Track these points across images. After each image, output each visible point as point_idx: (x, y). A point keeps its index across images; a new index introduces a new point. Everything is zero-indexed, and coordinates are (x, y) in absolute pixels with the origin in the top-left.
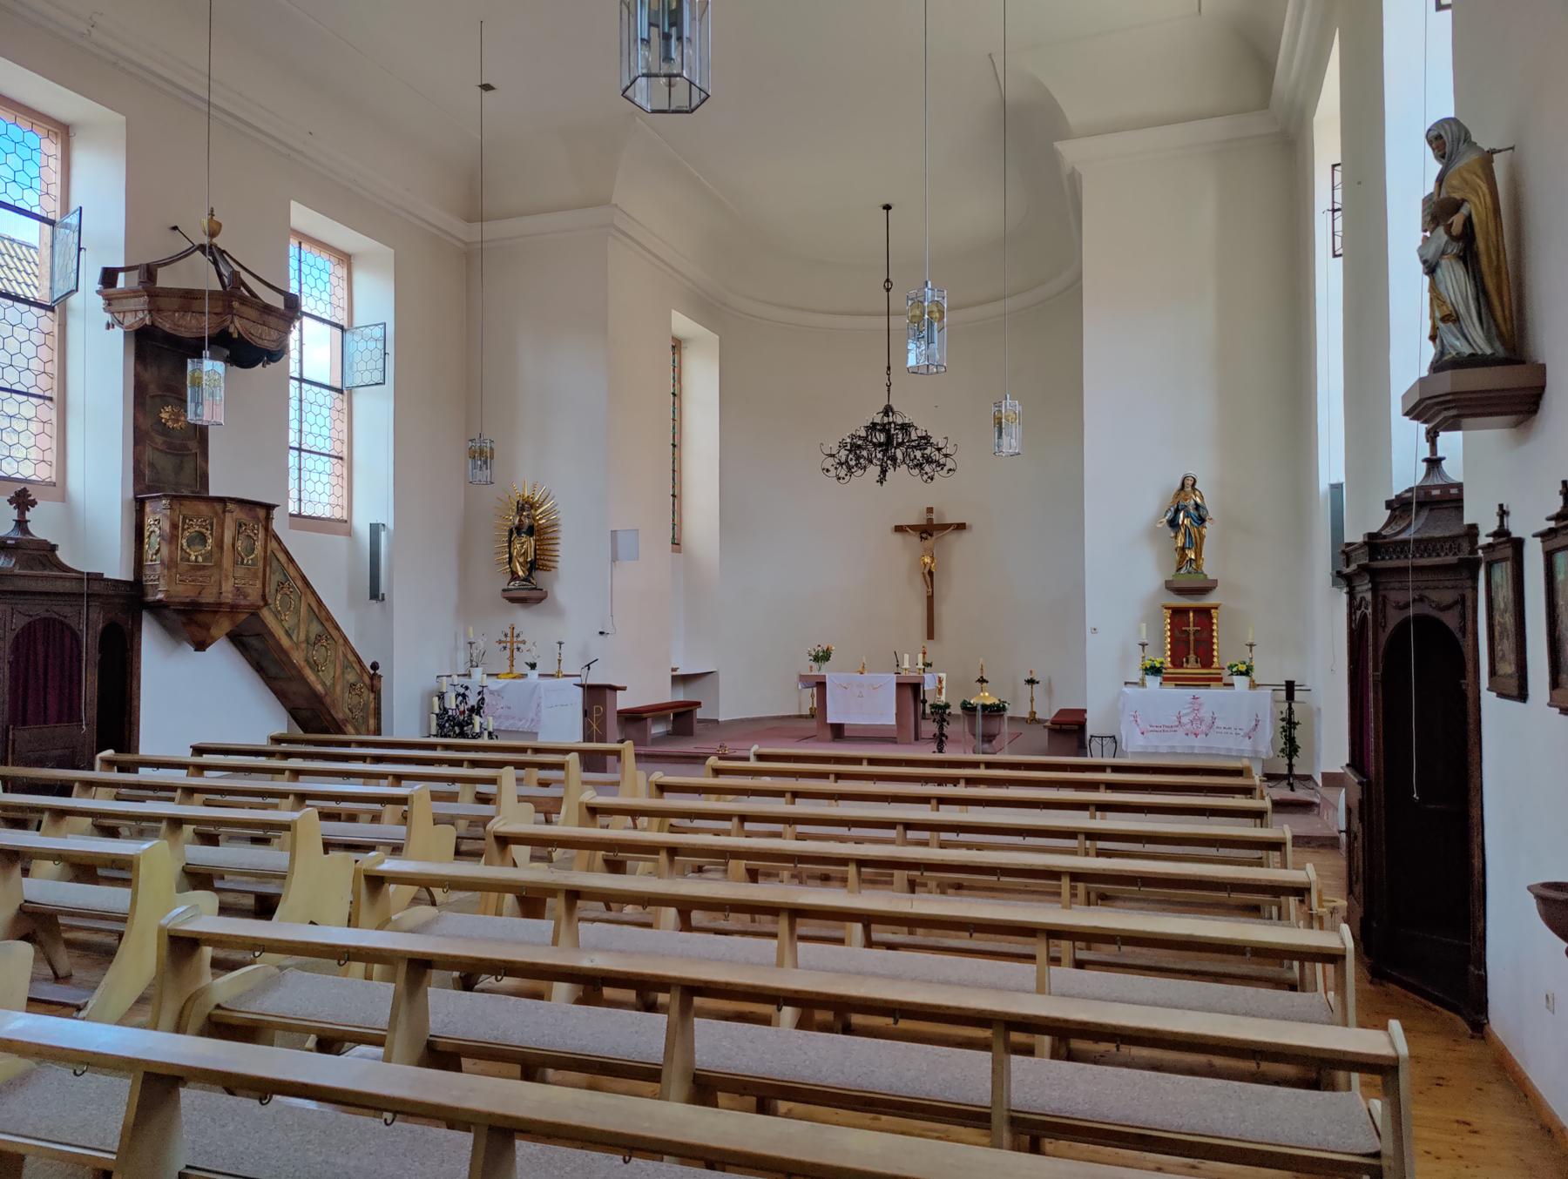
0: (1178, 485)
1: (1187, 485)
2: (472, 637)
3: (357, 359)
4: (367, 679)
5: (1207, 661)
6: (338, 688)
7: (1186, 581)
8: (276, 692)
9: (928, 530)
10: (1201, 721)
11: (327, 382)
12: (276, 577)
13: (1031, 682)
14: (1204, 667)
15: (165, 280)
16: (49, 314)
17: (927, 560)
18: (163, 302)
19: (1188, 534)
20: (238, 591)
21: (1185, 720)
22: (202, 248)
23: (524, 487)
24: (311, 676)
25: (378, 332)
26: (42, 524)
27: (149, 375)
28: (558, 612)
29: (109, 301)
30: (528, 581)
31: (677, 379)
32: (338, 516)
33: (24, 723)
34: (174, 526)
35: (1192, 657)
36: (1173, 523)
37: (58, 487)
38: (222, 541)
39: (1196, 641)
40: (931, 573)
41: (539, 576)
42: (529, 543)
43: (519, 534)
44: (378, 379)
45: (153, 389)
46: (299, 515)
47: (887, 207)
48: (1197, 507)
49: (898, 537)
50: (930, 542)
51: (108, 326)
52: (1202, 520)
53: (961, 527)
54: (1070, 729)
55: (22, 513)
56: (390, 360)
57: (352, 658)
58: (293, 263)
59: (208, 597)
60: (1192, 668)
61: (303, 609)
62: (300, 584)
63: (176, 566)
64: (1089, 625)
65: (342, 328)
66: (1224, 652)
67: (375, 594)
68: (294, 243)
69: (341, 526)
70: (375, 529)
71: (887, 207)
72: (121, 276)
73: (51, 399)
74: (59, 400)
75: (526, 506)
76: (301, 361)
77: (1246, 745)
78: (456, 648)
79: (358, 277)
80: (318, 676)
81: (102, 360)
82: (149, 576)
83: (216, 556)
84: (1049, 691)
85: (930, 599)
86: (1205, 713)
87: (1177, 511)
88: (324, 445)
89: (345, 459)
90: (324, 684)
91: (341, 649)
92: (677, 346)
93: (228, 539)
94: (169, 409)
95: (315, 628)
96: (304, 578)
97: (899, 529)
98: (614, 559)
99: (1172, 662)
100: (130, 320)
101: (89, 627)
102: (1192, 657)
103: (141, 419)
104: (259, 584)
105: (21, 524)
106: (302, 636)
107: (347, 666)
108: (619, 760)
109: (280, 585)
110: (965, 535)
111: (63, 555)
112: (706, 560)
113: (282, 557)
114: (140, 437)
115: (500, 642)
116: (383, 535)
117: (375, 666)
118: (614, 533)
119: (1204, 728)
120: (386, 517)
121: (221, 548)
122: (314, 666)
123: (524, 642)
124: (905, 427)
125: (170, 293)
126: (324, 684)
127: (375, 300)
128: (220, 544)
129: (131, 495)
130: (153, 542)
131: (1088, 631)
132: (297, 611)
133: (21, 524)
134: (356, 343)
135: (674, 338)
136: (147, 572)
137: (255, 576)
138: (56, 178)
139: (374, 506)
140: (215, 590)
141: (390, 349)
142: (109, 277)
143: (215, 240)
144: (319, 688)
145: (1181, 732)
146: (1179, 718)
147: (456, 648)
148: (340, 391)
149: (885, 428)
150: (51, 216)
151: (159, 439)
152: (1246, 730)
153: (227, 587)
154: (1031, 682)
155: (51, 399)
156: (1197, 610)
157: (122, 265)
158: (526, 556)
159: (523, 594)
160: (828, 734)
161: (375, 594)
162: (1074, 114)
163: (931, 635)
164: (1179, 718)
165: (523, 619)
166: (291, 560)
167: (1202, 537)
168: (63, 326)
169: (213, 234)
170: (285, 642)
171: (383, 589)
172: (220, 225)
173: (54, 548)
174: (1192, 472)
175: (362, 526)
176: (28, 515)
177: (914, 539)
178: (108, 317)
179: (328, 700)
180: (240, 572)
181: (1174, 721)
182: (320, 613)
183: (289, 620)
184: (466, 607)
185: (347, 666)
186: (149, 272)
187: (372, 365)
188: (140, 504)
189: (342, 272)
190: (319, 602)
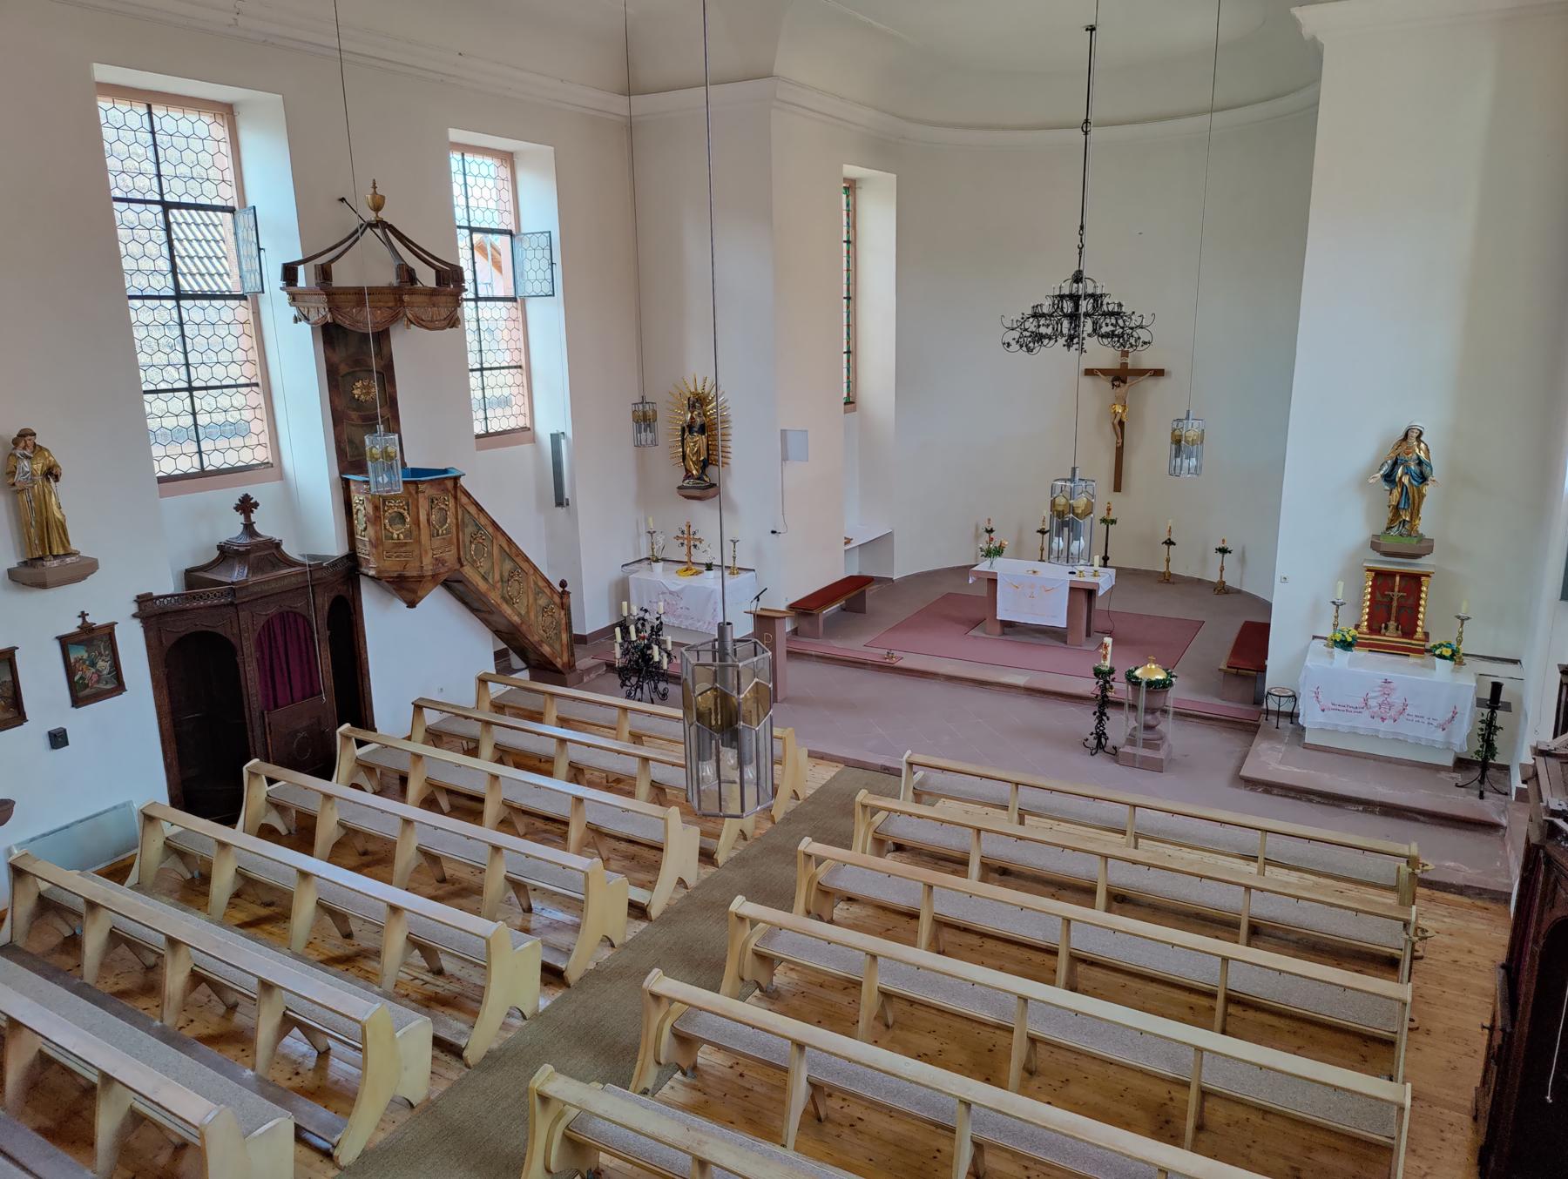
0: (1401, 435)
1: (1410, 437)
2: (652, 527)
3: (527, 267)
4: (557, 599)
5: (1409, 632)
6: (532, 615)
7: (1394, 540)
9: (1120, 376)
10: (1391, 706)
11: (502, 294)
12: (470, 529)
13: (1223, 551)
14: (1405, 635)
15: (343, 276)
16: (243, 303)
19: (1405, 491)
20: (439, 561)
21: (1372, 703)
22: (371, 225)
23: (697, 375)
25: (544, 240)
26: (266, 525)
27: (340, 355)
29: (294, 298)
30: (702, 476)
31: (852, 225)
32: (522, 424)
33: (276, 706)
34: (376, 508)
35: (1392, 624)
36: (1389, 478)
37: (272, 468)
39: (1400, 607)
40: (1121, 423)
41: (711, 470)
43: (691, 432)
44: (547, 290)
45: (343, 369)
46: (487, 434)
47: (1092, 29)
48: (1420, 462)
49: (1088, 380)
50: (1124, 388)
51: (296, 320)
52: (1423, 479)
53: (1159, 373)
55: (248, 518)
56: (558, 270)
57: (541, 583)
58: (457, 179)
59: (412, 572)
60: (1391, 636)
61: (496, 550)
62: (490, 529)
65: (510, 233)
67: (560, 501)
68: (455, 158)
69: (525, 433)
70: (556, 439)
71: (1092, 29)
72: (301, 269)
73: (257, 385)
74: (263, 384)
75: (698, 401)
76: (475, 281)
77: (1439, 736)
78: (639, 535)
79: (522, 177)
80: (513, 609)
81: (296, 354)
82: (364, 551)
83: (415, 533)
84: (1242, 560)
85: (1119, 452)
86: (1397, 699)
87: (1395, 464)
88: (505, 359)
89: (523, 368)
90: (519, 615)
91: (532, 578)
92: (851, 187)
93: (423, 518)
94: (359, 384)
95: (508, 566)
96: (494, 523)
97: (1089, 372)
98: (785, 459)
99: (1369, 627)
100: (314, 317)
101: (318, 610)
102: (1392, 624)
103: (337, 401)
104: (454, 551)
105: (249, 527)
106: (497, 577)
107: (539, 592)
109: (473, 538)
110: (1162, 382)
111: (291, 550)
112: (878, 412)
113: (472, 509)
115: (678, 538)
116: (563, 442)
117: (563, 584)
118: (783, 432)
119: (1393, 713)
120: (564, 424)
122: (509, 600)
123: (700, 541)
124: (1096, 298)
125: (345, 291)
126: (519, 615)
127: (540, 208)
128: (417, 522)
130: (360, 522)
131: (1277, 579)
132: (491, 554)
133: (249, 527)
134: (524, 245)
135: (845, 180)
136: (359, 545)
137: (450, 543)
138: (227, 162)
139: (553, 416)
141: (557, 258)
142: (289, 273)
143: (380, 214)
144: (516, 619)
145: (1366, 713)
146: (1366, 700)
147: (639, 535)
148: (514, 299)
149: (1075, 298)
150: (230, 204)
151: (354, 415)
152: (1441, 722)
153: (427, 561)
154: (1223, 551)
155: (257, 385)
156: (1403, 575)
157: (300, 257)
158: (696, 450)
159: (697, 493)
160: (998, 628)
161: (560, 501)
163: (1117, 487)
164: (1366, 700)
165: (703, 516)
166: (481, 510)
167: (1421, 496)
168: (257, 313)
169: (377, 208)
170: (482, 586)
171: (567, 495)
172: (383, 198)
173: (278, 545)
174: (1419, 424)
175: (544, 431)
176: (253, 517)
177: (1105, 383)
178: (293, 311)
179: (524, 628)
180: (437, 542)
181: (1359, 702)
182: (512, 552)
183: (484, 565)
184: (645, 496)
185: (539, 592)
186: (325, 273)
187: (540, 275)
189: (505, 172)
190: (509, 541)
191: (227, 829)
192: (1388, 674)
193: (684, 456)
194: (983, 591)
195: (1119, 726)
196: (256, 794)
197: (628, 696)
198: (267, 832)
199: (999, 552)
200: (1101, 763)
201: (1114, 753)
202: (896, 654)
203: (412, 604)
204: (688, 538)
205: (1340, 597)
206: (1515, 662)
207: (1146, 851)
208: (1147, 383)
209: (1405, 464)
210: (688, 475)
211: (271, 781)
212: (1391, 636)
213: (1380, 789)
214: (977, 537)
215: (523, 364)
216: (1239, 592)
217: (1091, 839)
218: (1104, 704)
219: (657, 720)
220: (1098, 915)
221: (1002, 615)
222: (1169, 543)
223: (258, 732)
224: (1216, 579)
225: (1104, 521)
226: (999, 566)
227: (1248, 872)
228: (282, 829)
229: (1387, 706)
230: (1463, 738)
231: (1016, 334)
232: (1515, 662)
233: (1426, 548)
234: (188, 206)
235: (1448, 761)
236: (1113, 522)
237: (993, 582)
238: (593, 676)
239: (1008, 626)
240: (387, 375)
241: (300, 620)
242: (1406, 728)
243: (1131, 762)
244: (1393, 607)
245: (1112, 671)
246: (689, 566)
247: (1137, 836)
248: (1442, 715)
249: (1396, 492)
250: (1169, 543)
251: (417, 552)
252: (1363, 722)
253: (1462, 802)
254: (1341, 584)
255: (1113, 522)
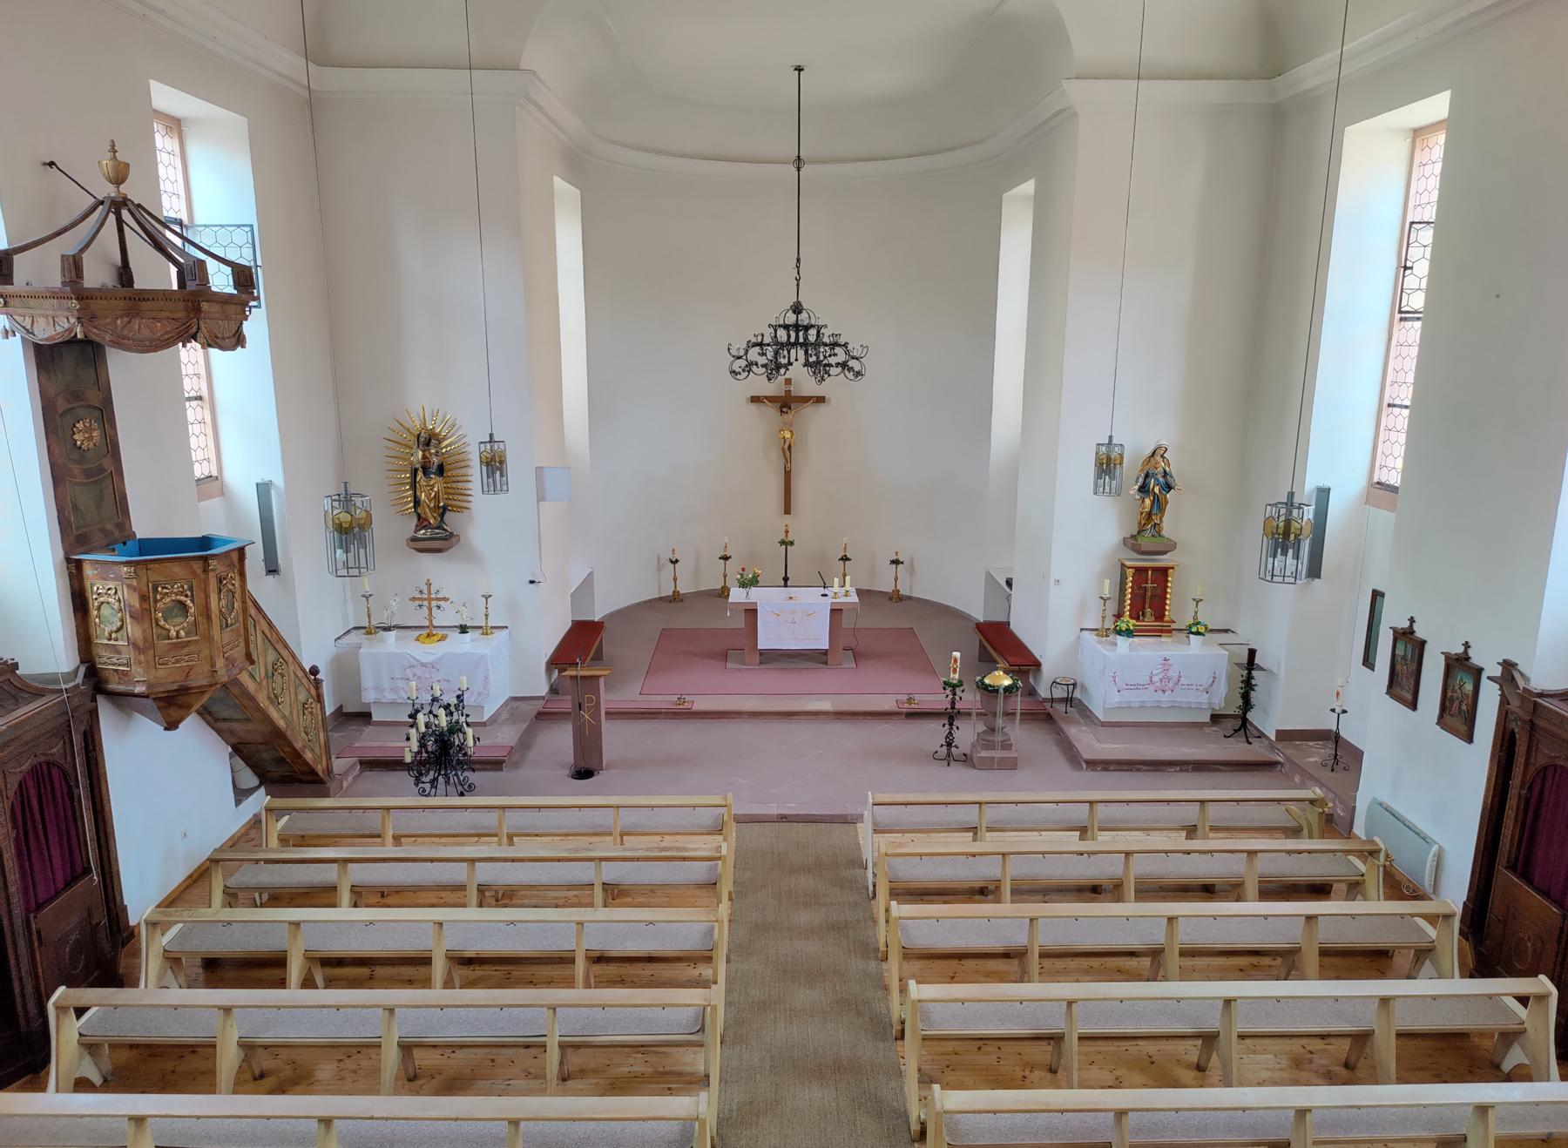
0: (1149, 451)
5: (1160, 615)
7: (1146, 541)
8: (219, 732)
13: (896, 562)
17: (788, 435)
18: (95, 305)
21: (1155, 679)
24: (274, 714)
28: (473, 558)
30: (435, 530)
34: (144, 598)
36: (1143, 489)
38: (207, 607)
42: (437, 484)
45: (62, 405)
47: (799, 69)
49: (754, 407)
50: (789, 417)
54: (998, 642)
59: (199, 679)
60: (1149, 621)
63: (153, 646)
64: (1054, 575)
66: (1178, 609)
70: (263, 490)
71: (799, 69)
75: (428, 440)
77: (1204, 698)
79: (193, 150)
80: (279, 711)
84: (912, 570)
86: (1173, 673)
87: (1147, 476)
90: (284, 717)
91: (292, 668)
94: (80, 425)
97: (755, 400)
98: (541, 498)
108: (1075, 1001)
110: (822, 407)
114: (59, 476)
115: (414, 599)
118: (539, 470)
120: (275, 474)
121: (209, 618)
126: (284, 717)
128: (206, 613)
129: (61, 554)
140: (207, 668)
143: (123, 188)
144: (281, 723)
145: (1151, 688)
154: (896, 562)
156: (1155, 569)
162: (1084, 45)
163: (787, 510)
165: (438, 571)
169: (119, 178)
177: (771, 411)
179: (289, 734)
188: (74, 573)
191: (39, 1095)
192: (1166, 654)
193: (417, 502)
194: (740, 622)
195: (966, 734)
196: (66, 1036)
197: (423, 793)
198: (82, 1085)
199: (754, 582)
200: (958, 772)
201: (967, 760)
202: (688, 698)
203: (171, 725)
204: (428, 598)
205: (1106, 593)
206: (1226, 631)
207: (524, 848)
208: (809, 410)
209: (1154, 475)
210: (422, 522)
211: (80, 1012)
212: (1149, 621)
213: (1184, 750)
214: (660, 568)
215: (205, 393)
216: (910, 598)
217: (901, 845)
218: (951, 716)
219: (552, 814)
220: (472, 913)
221: (763, 643)
222: (675, 562)
223: (23, 949)
224: (889, 588)
225: (783, 543)
226: (756, 595)
227: (963, 842)
228: (96, 1079)
229: (1168, 682)
230: (1222, 697)
231: (743, 363)
232: (1226, 631)
233: (1170, 547)
234: (540, 108)
235: (1207, 719)
236: (792, 543)
237: (751, 612)
238: (350, 779)
239: (763, 653)
240: (105, 413)
241: (55, 773)
242: (1182, 697)
243: (989, 765)
244: (1144, 597)
245: (960, 684)
246: (429, 632)
247: (510, 837)
248: (1206, 681)
249: (1148, 501)
250: (845, 559)
251: (206, 652)
252: (1149, 696)
253: (1236, 750)
254: (1107, 582)
255: (792, 543)
